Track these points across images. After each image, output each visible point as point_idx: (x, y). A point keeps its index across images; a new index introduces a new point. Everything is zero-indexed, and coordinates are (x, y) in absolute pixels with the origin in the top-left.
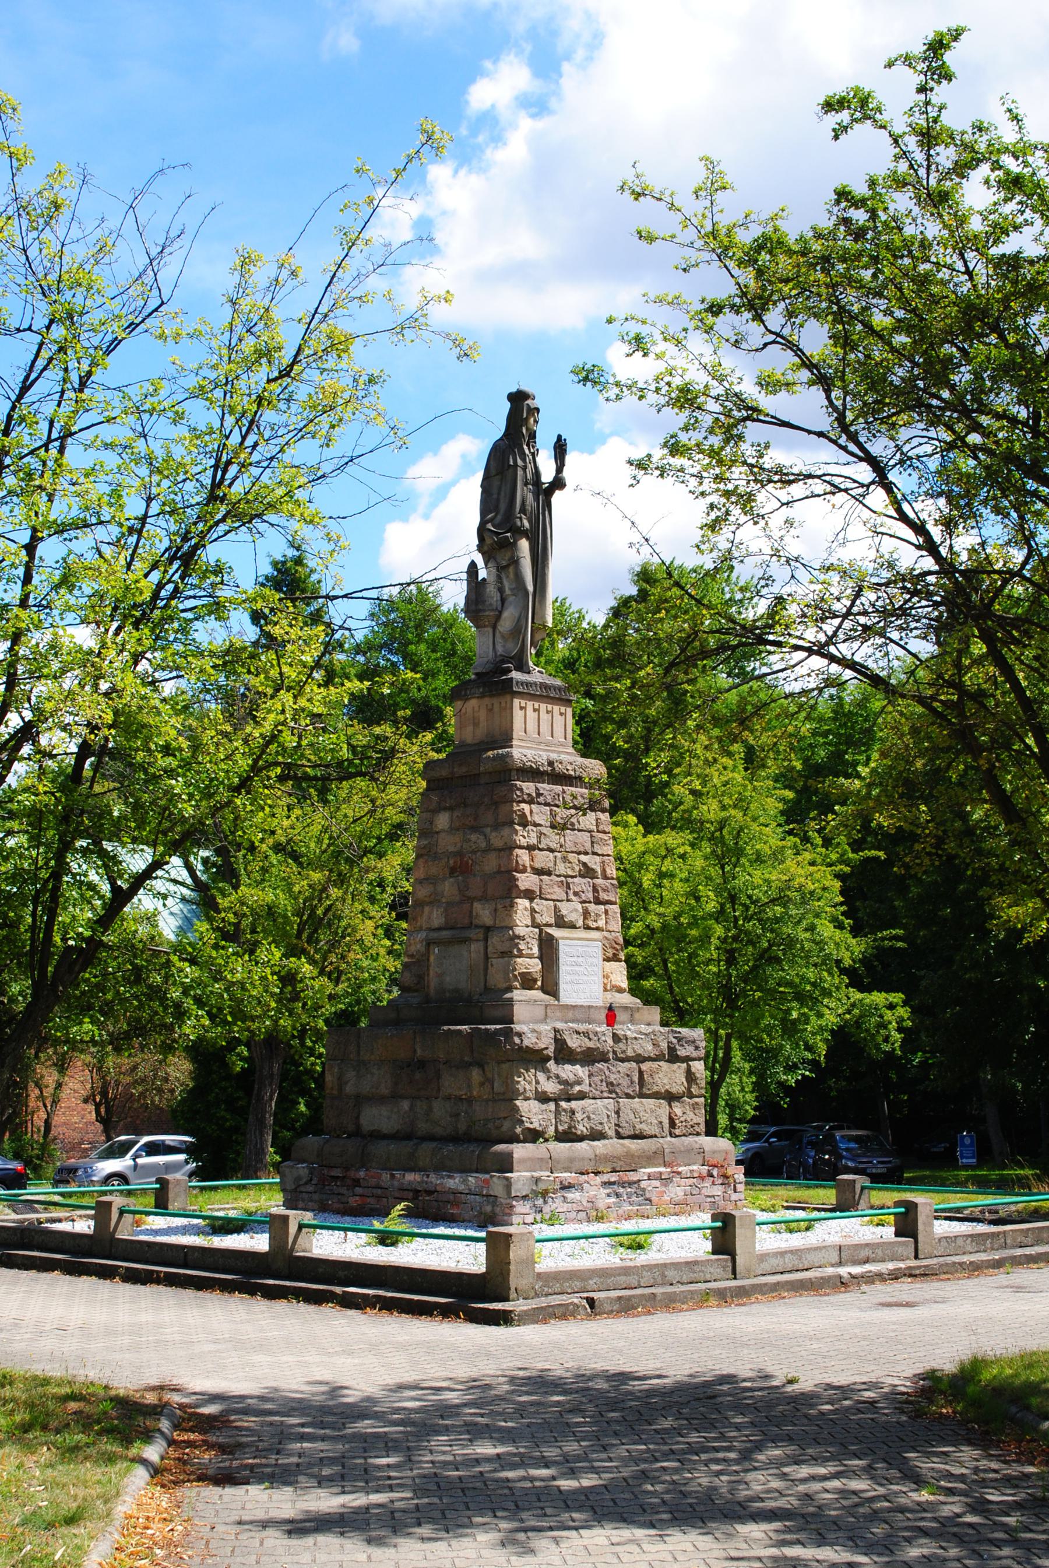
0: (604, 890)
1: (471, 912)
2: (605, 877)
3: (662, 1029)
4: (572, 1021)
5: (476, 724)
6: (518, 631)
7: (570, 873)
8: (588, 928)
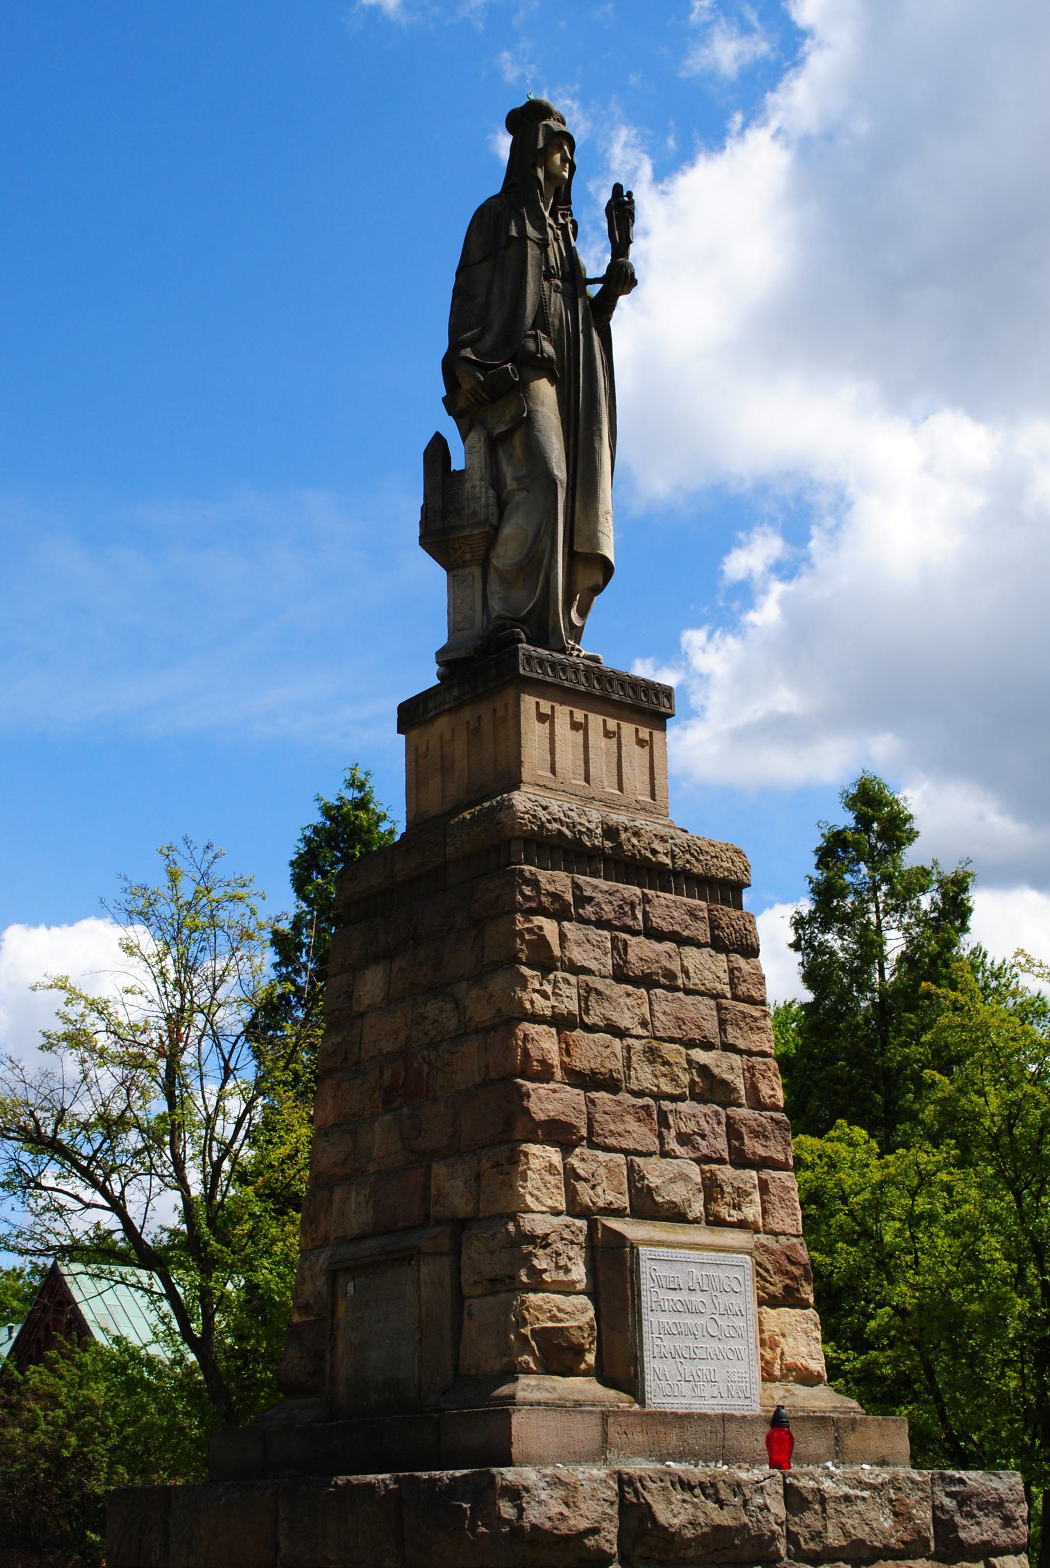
0: (756, 1134)
1: (427, 1188)
2: (757, 1103)
3: (915, 1475)
4: (679, 1457)
5: (446, 771)
6: (535, 562)
7: (667, 1087)
8: (717, 1222)
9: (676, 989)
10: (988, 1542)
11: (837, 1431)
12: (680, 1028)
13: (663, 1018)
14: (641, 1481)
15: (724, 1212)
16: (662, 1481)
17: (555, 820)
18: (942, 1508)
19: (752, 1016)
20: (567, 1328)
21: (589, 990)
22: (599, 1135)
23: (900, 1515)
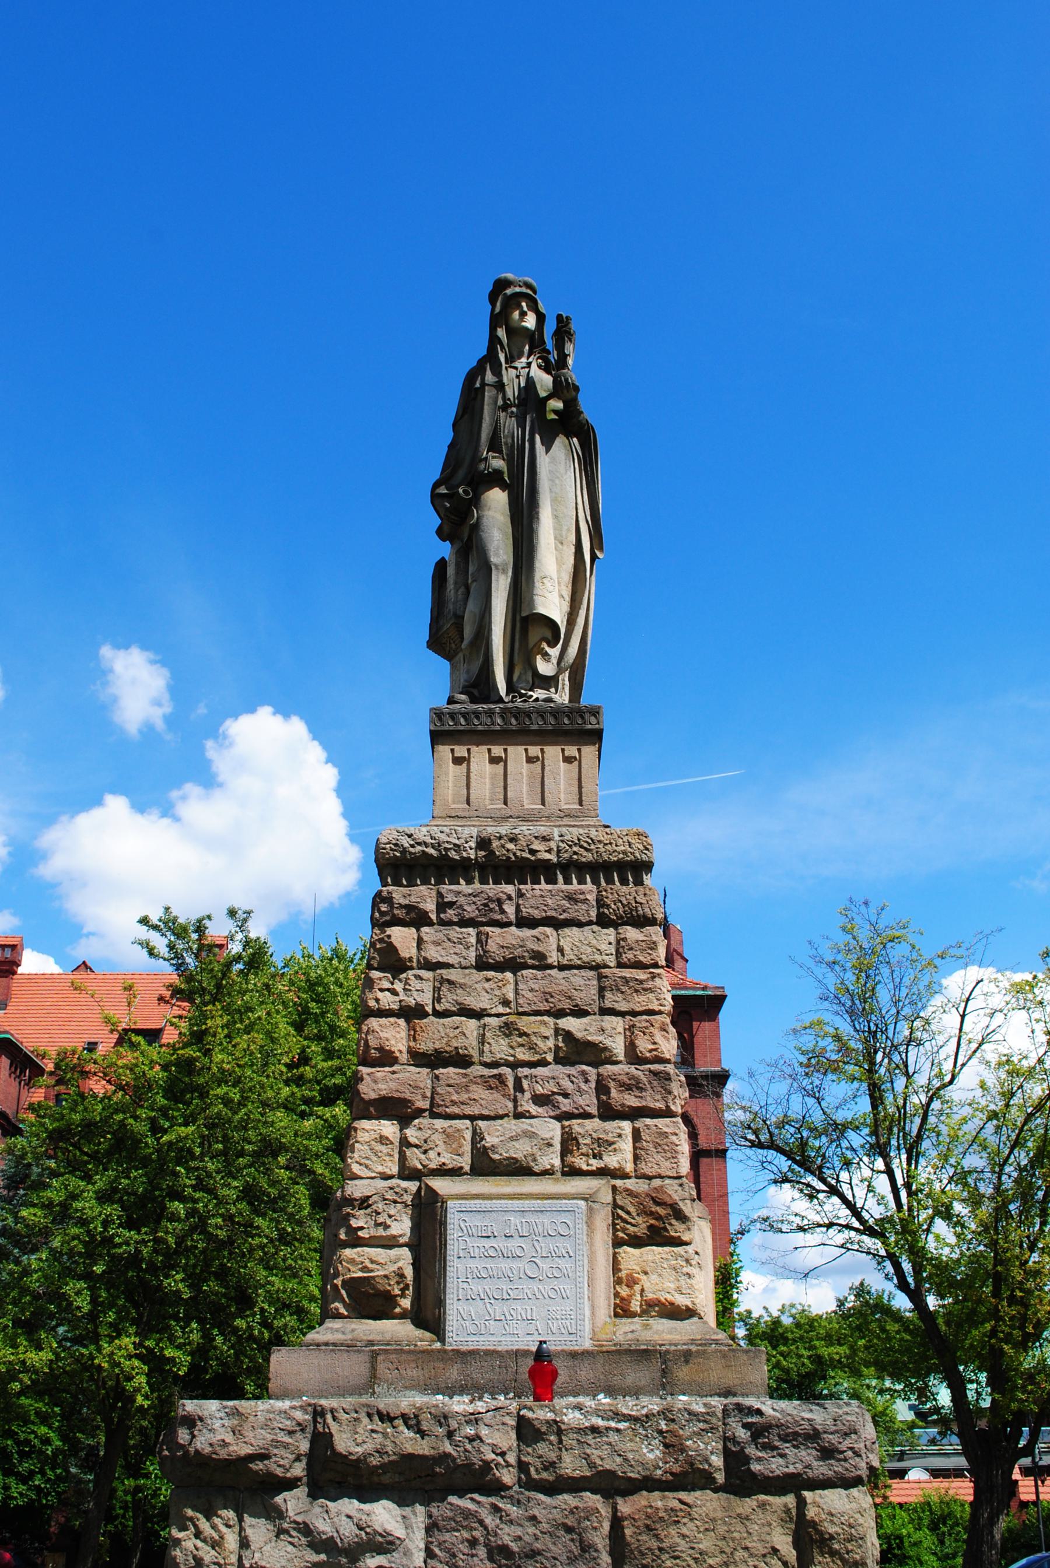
7: (523, 1055)
8: (572, 1172)
9: (551, 967)
10: (799, 1475)
11: (665, 1362)
12: (547, 1000)
13: (529, 995)
14: (332, 1412)
15: (581, 1163)
16: (356, 1412)
17: (419, 844)
18: (734, 1440)
19: (636, 980)
20: (373, 1278)
21: (443, 981)
22: (439, 1106)
23: (672, 1446)
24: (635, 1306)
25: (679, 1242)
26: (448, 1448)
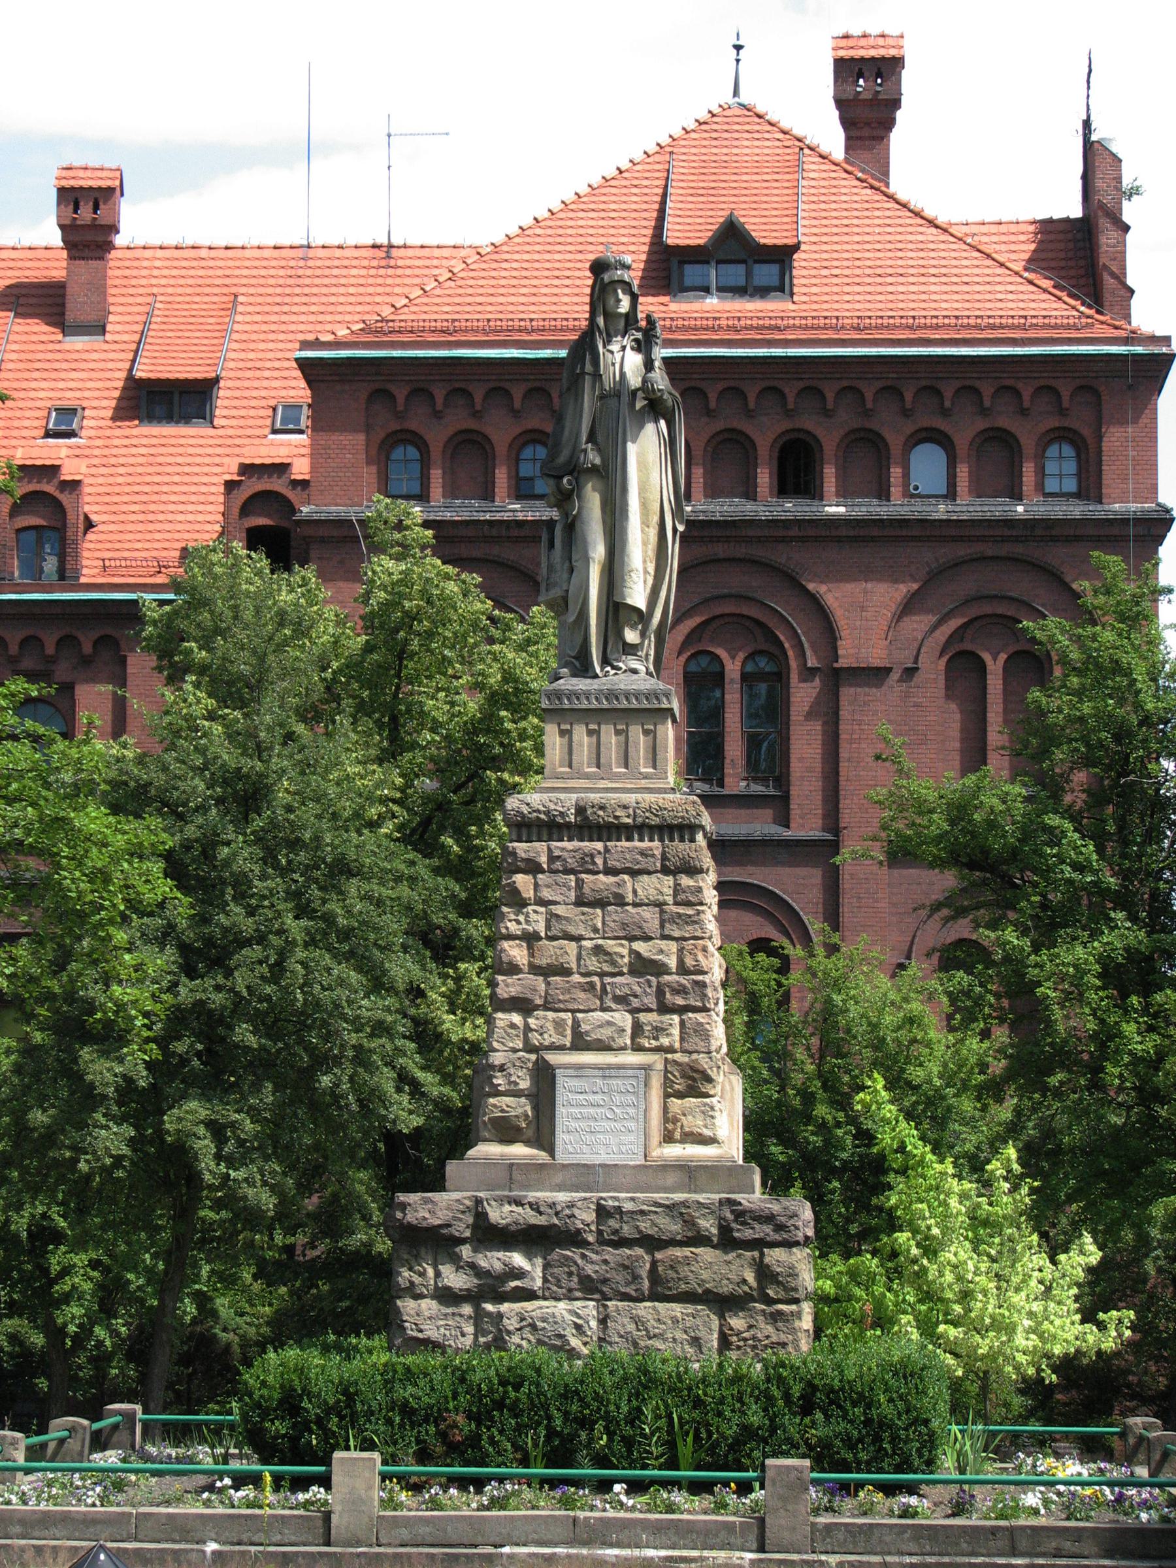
24: (677, 1135)
25: (708, 1096)
26: (556, 1222)
